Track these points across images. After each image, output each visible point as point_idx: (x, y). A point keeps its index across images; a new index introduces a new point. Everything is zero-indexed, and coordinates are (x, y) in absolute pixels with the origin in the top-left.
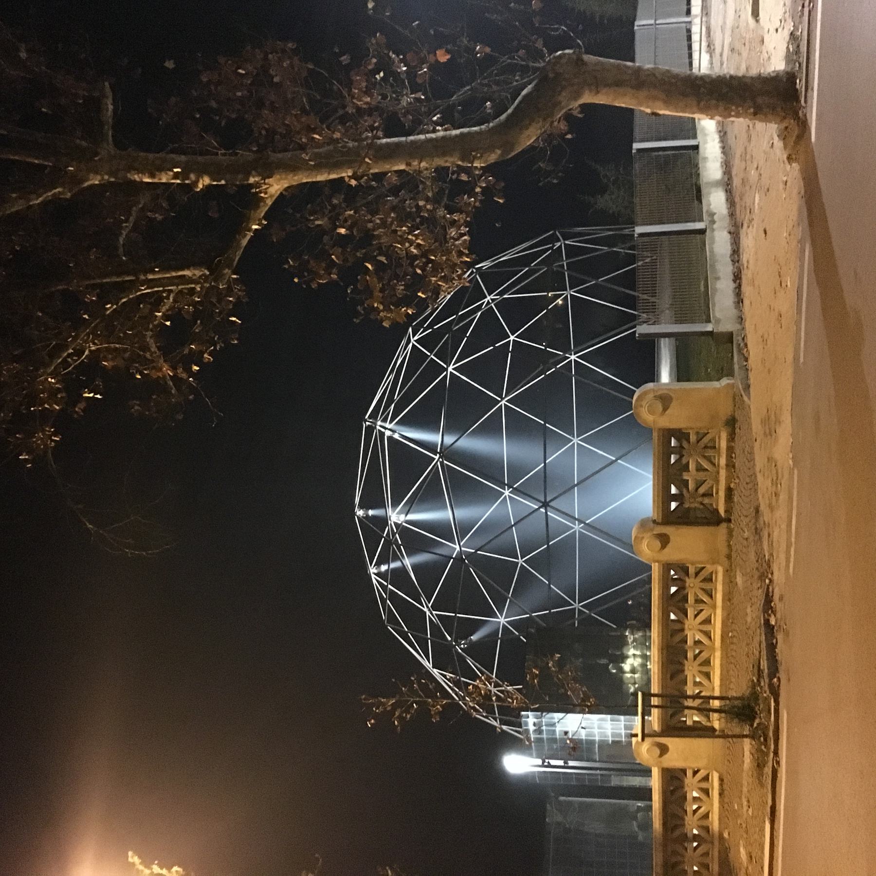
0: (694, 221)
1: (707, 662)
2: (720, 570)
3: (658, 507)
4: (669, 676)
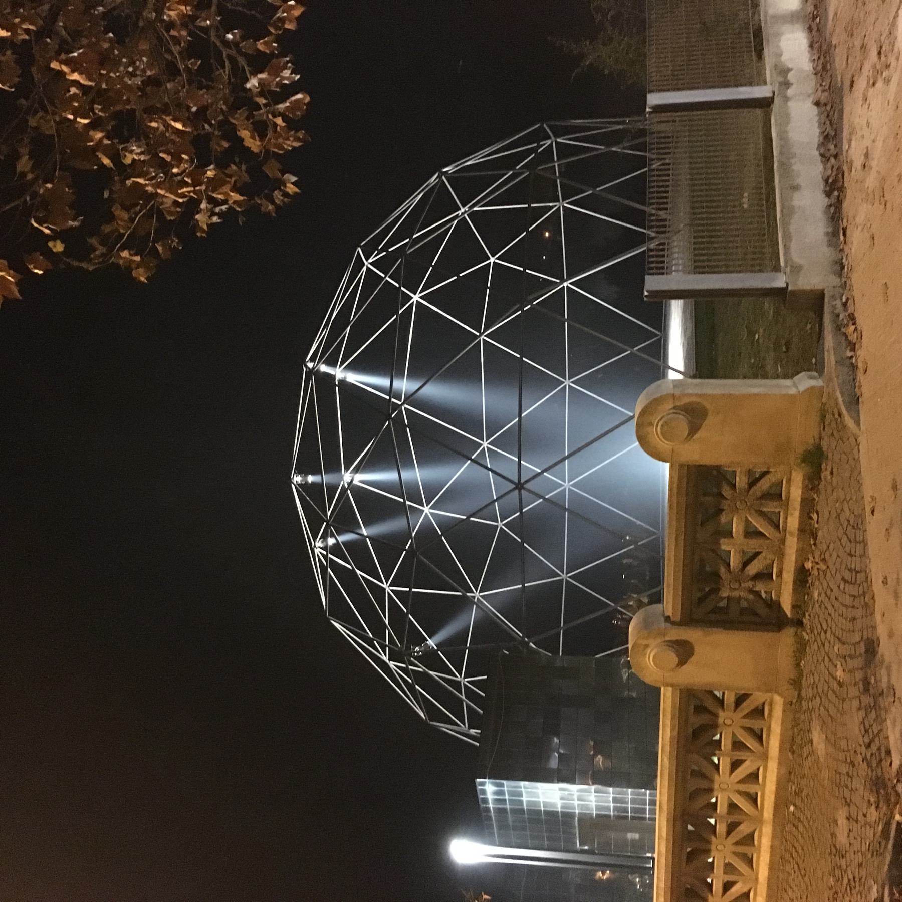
0: (750, 84)
1: (749, 840)
2: (779, 701)
4: (684, 857)
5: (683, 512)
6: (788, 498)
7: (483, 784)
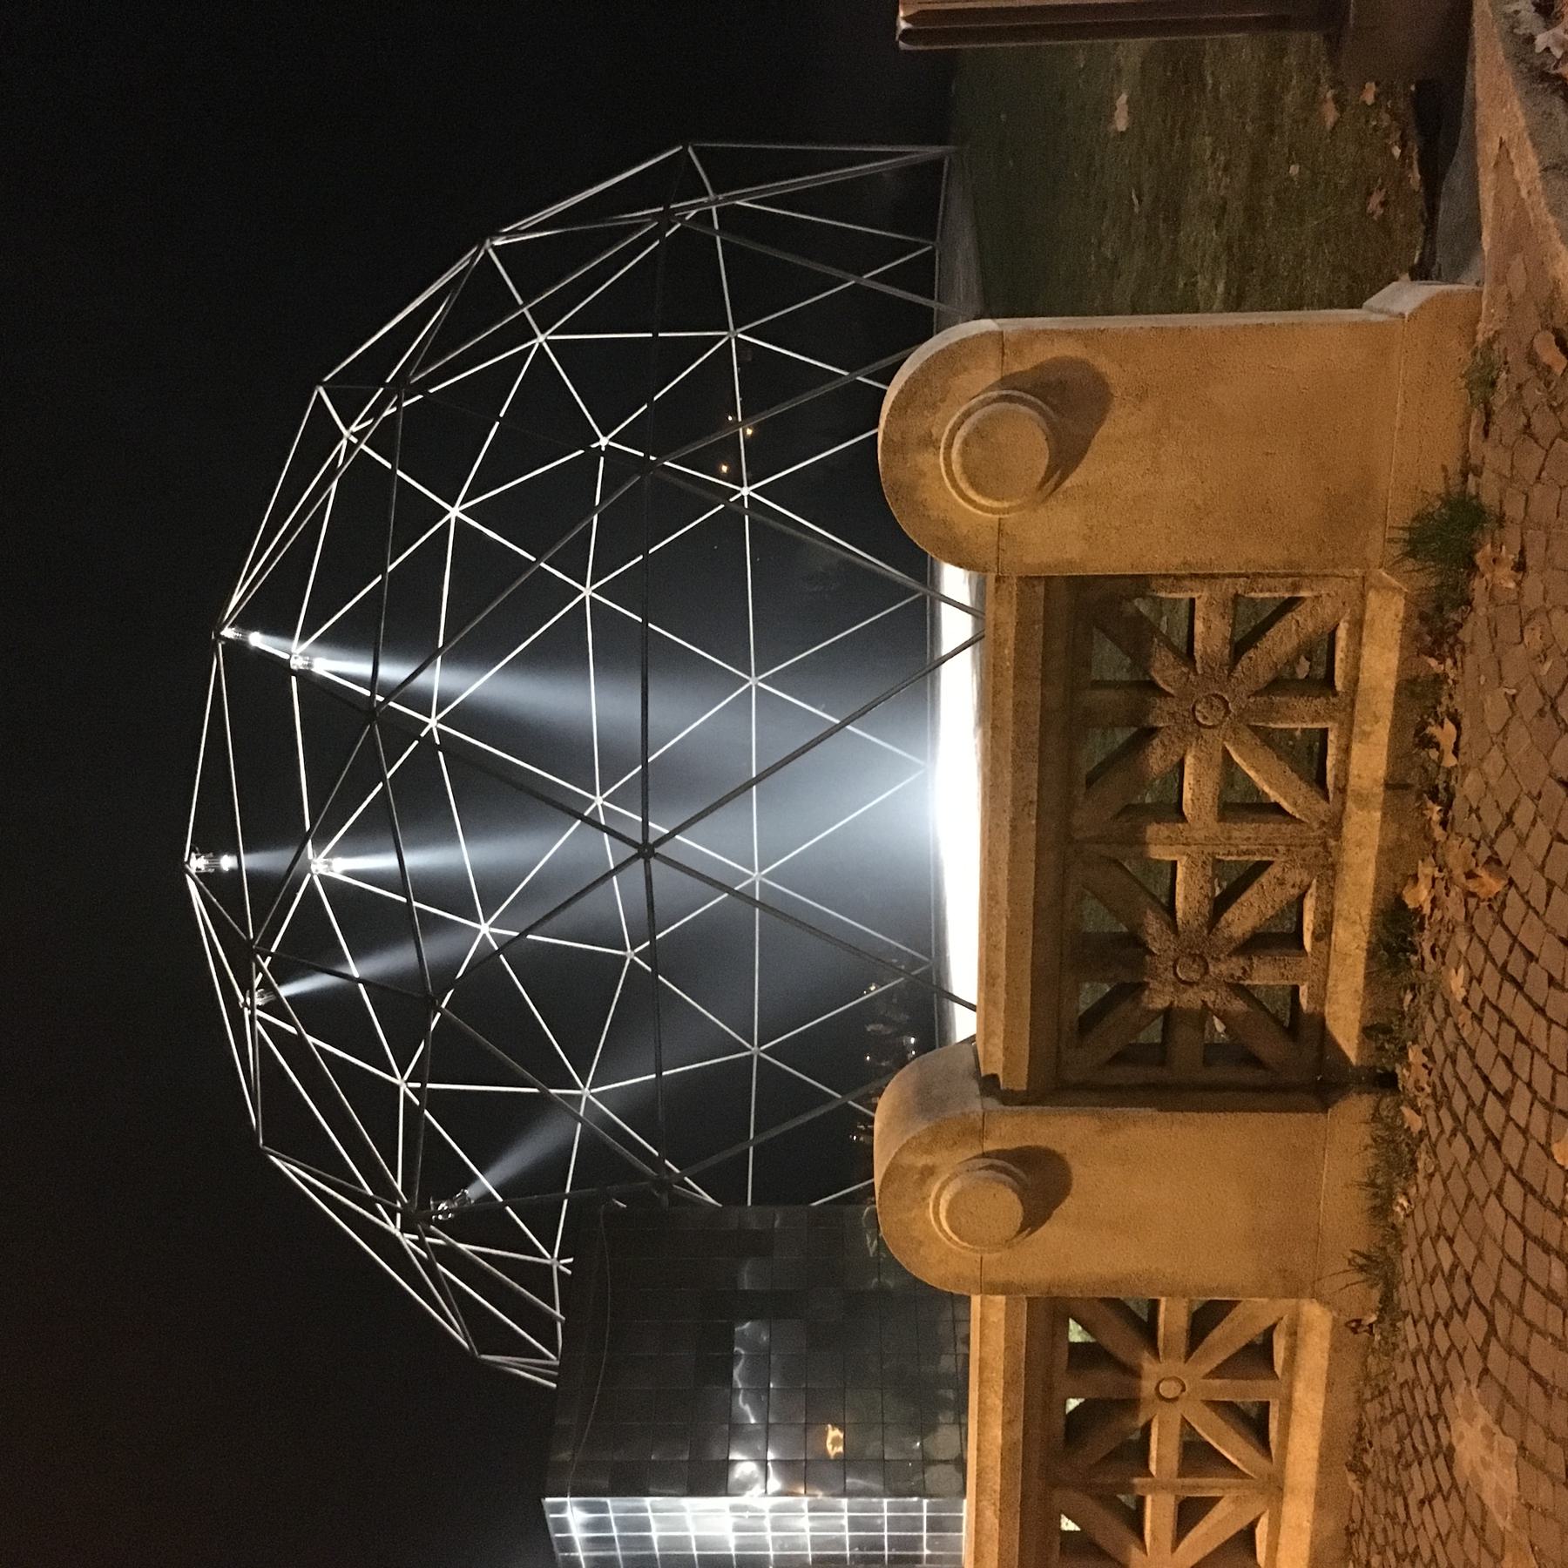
2: (1317, 1319)
3: (1011, 1010)
5: (1035, 738)
6: (1354, 682)
7: (560, 1508)
